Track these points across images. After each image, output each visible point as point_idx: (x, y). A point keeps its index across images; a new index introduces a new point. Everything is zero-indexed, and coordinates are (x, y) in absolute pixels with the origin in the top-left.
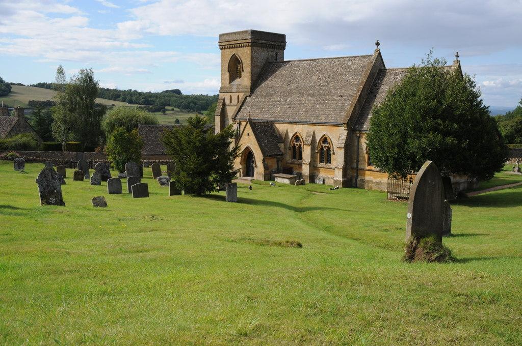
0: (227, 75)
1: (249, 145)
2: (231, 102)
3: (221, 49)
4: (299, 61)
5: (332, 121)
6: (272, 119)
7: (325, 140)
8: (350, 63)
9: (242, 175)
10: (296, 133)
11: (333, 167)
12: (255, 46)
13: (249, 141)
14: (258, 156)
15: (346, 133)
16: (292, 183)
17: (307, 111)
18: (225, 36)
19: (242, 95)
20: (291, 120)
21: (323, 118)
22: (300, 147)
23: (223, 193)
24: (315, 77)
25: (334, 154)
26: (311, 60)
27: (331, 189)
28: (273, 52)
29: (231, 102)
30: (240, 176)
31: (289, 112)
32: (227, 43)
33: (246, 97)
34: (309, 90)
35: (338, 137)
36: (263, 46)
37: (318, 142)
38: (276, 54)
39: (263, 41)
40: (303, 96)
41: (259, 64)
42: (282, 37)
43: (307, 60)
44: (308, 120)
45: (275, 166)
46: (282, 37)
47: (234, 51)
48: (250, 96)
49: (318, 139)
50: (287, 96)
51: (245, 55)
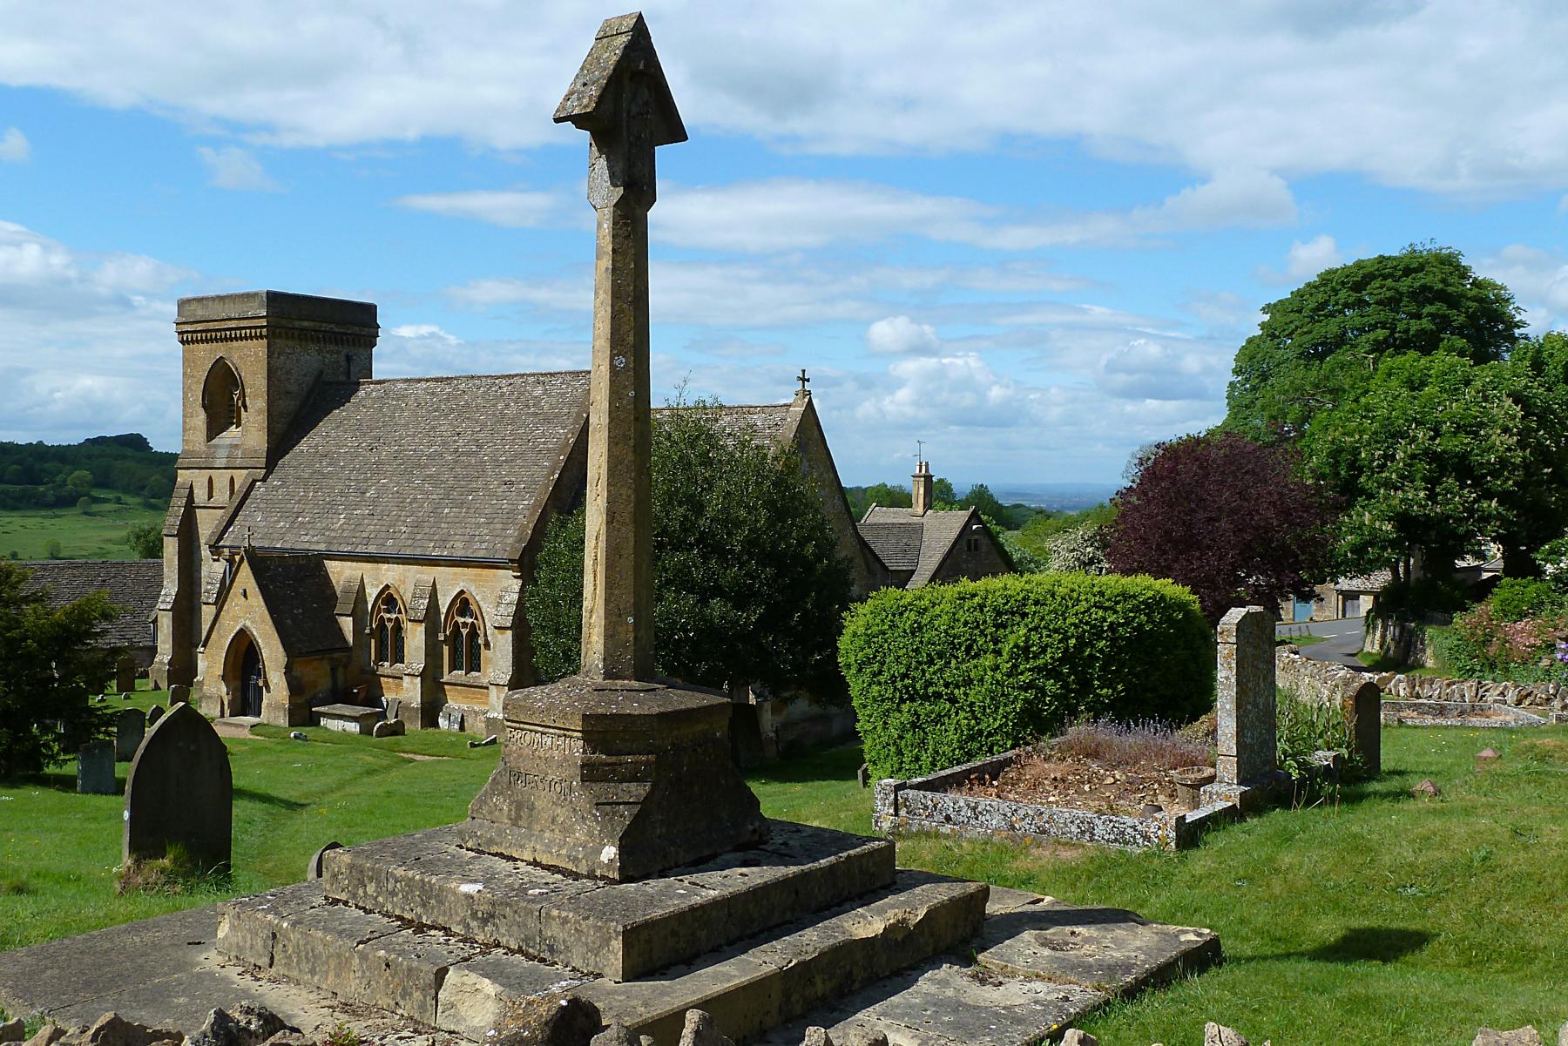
0: (200, 419)
1: (248, 623)
2: (210, 496)
3: (182, 342)
4: (407, 380)
5: (481, 554)
6: (322, 547)
7: (463, 604)
8: (539, 391)
9: (227, 712)
10: (387, 587)
11: (485, 682)
12: (280, 336)
13: (247, 611)
14: (272, 654)
15: (516, 585)
16: (366, 731)
17: (417, 525)
18: (193, 306)
19: (241, 477)
20: (372, 549)
21: (459, 545)
22: (398, 628)
23: (72, 768)
24: (444, 428)
25: (487, 645)
26: (436, 380)
27: (473, 745)
28: (338, 353)
29: (210, 496)
30: (222, 715)
31: (370, 529)
32: (200, 327)
33: (254, 481)
34: (426, 466)
35: (496, 596)
36: (304, 336)
37: (444, 610)
38: (348, 359)
39: (306, 324)
40: (409, 482)
41: (294, 388)
42: (369, 311)
43: (427, 380)
44: (418, 551)
45: (325, 684)
46: (369, 311)
47: (219, 350)
48: (264, 480)
49: (444, 604)
50: (366, 480)
51: (251, 361)
